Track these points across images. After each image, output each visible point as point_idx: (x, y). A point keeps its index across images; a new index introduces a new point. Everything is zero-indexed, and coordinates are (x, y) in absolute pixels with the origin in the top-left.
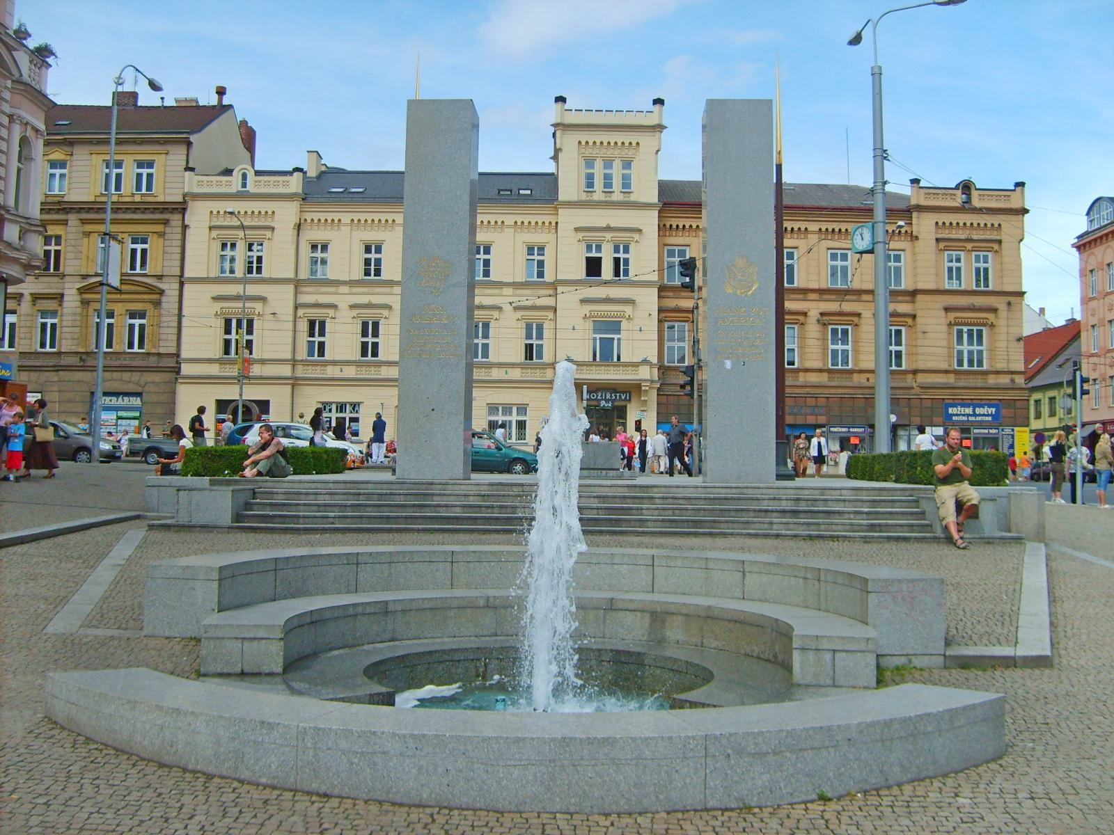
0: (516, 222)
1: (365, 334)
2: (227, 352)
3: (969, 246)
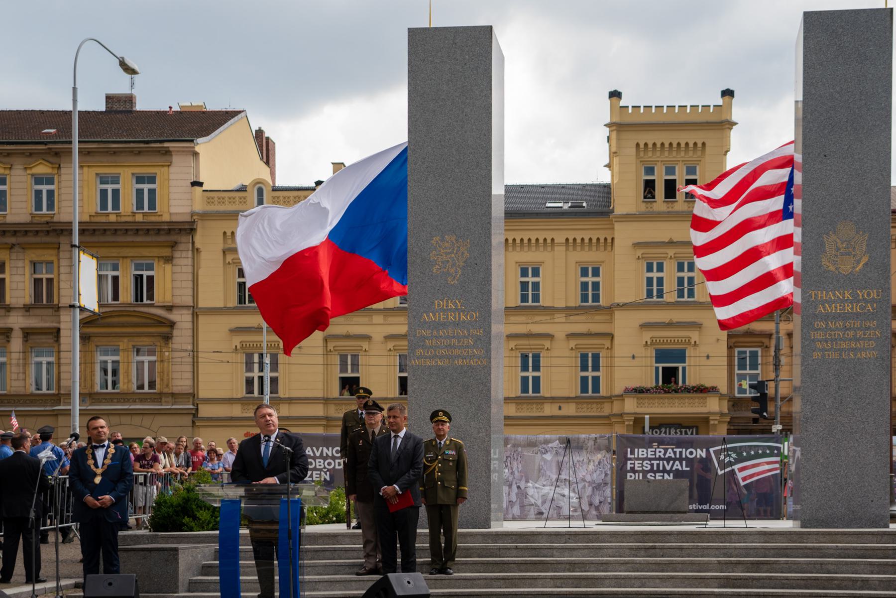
1: (584, 368)
2: (250, 391)
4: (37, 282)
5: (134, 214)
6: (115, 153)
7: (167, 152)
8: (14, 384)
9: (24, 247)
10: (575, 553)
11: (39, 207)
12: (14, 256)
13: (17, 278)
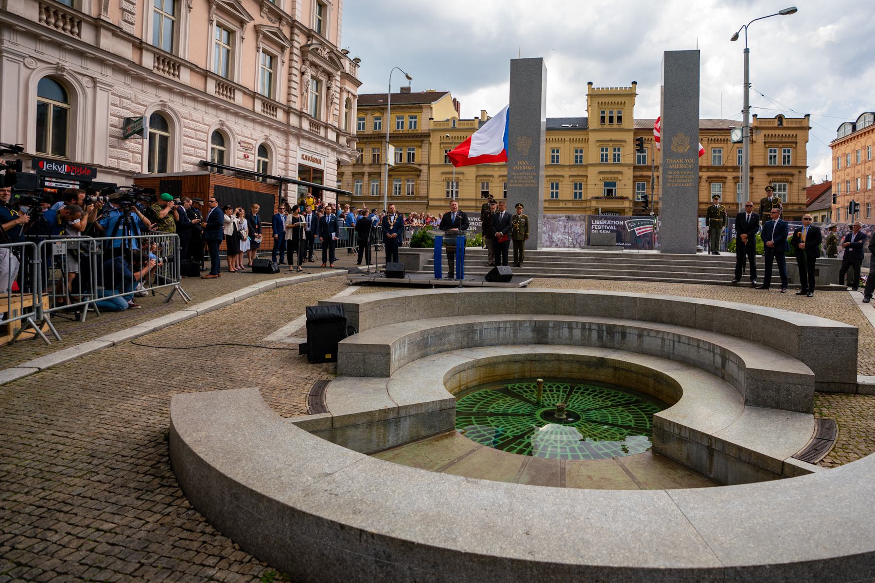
1: (576, 189)
2: (448, 196)
3: (781, 145)
4: (374, 155)
6: (403, 108)
7: (421, 108)
9: (370, 143)
11: (376, 128)
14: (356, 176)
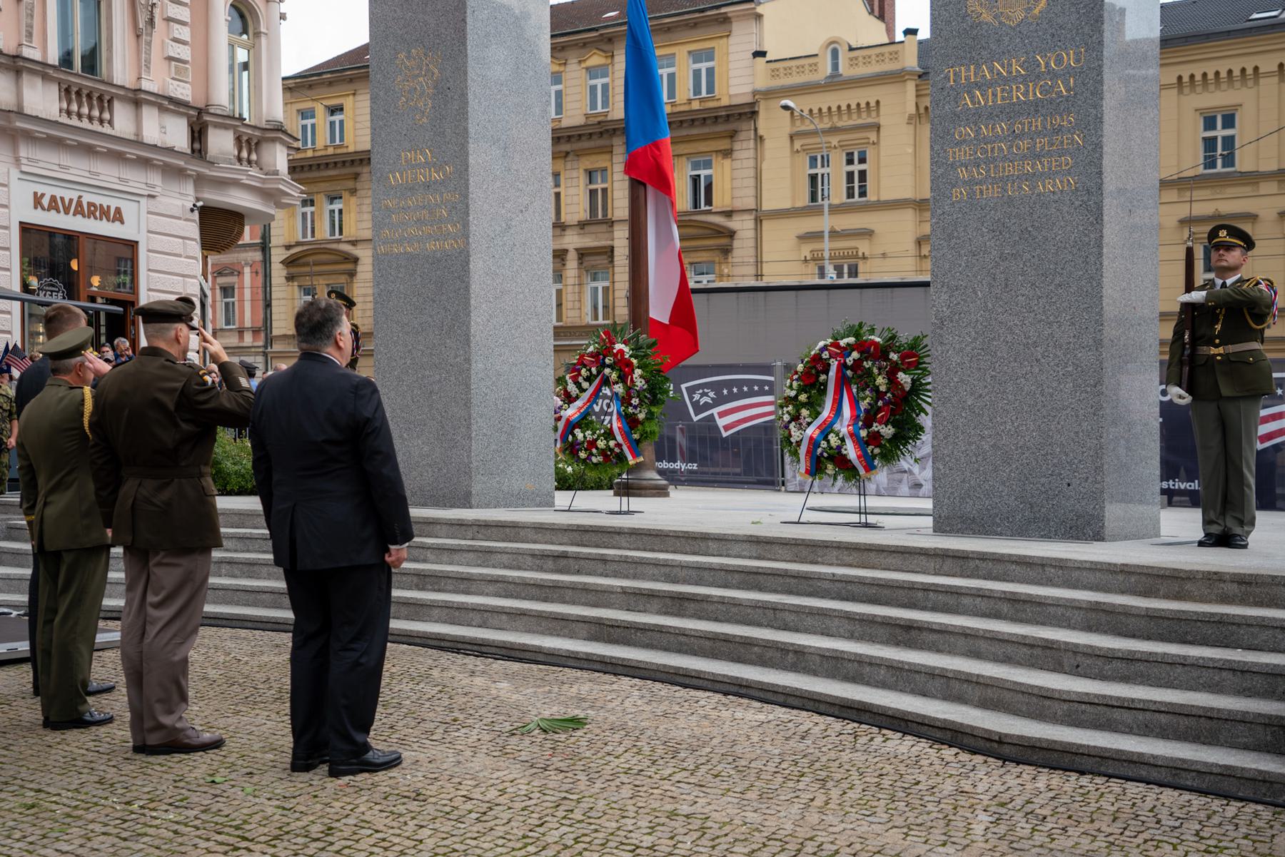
0: (1180, 78)
4: (593, 193)
5: (690, 101)
7: (726, 20)
8: (571, 313)
9: (579, 154)
10: (456, 557)
11: (593, 105)
12: (569, 165)
13: (572, 191)
14: (591, 261)
